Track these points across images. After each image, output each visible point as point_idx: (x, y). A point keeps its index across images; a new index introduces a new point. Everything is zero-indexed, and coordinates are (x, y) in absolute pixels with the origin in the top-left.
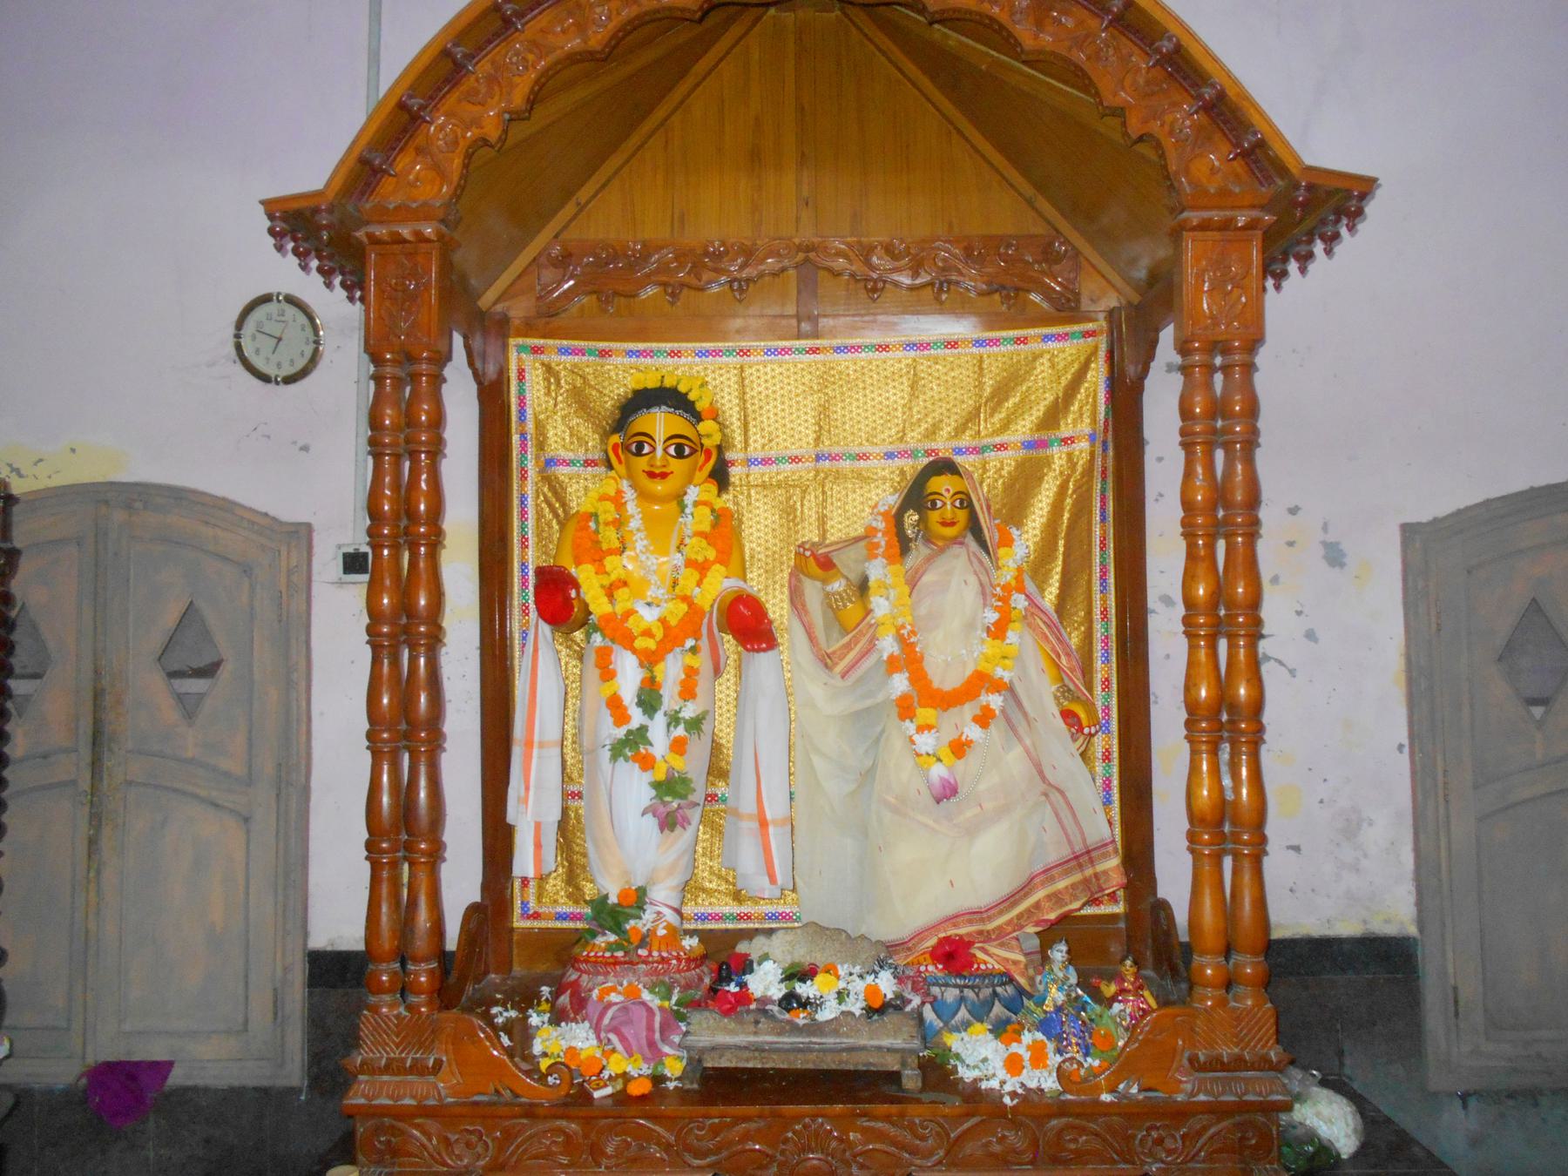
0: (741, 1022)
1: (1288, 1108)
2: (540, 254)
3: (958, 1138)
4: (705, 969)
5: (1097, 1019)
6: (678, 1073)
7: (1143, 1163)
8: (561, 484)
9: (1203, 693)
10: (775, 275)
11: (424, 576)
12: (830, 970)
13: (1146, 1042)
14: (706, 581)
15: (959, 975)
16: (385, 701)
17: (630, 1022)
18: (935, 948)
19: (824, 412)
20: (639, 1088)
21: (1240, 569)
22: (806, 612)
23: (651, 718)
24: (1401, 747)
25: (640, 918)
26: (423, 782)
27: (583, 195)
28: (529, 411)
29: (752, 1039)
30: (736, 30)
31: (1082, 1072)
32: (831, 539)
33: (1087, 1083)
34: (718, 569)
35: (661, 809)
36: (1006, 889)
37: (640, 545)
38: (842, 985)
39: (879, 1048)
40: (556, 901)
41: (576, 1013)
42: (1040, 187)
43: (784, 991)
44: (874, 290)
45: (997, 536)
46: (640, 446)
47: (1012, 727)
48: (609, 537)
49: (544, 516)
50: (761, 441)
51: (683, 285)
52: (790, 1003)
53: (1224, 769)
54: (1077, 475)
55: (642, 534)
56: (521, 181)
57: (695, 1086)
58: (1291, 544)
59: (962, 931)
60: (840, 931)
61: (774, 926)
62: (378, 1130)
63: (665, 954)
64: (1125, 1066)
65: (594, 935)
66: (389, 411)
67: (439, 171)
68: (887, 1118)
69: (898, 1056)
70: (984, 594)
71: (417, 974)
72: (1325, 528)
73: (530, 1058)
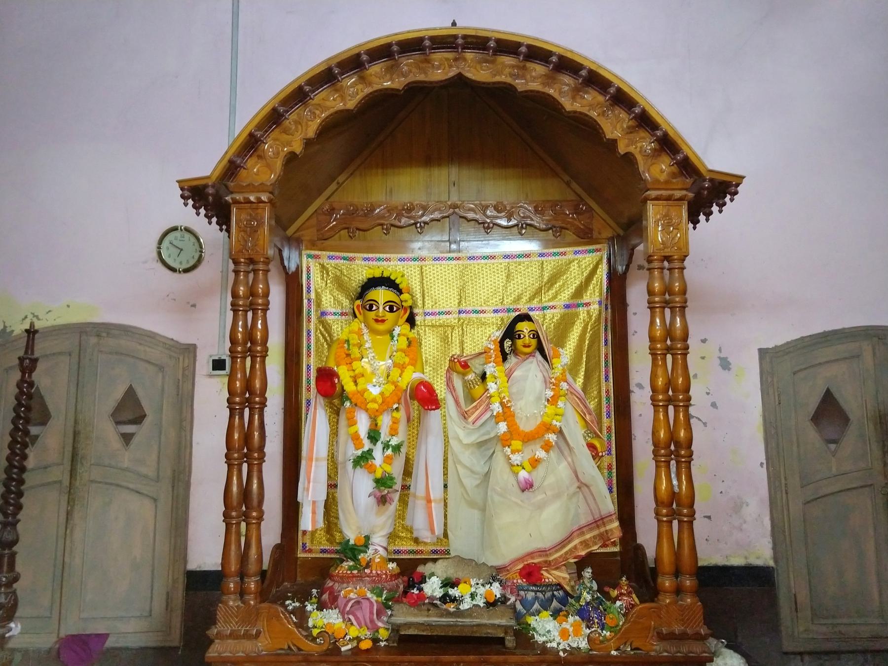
0: (421, 611)
8: (328, 324)
15: (535, 585)
19: (462, 290)
20: (366, 645)
21: (680, 372)
23: (375, 444)
24: (762, 464)
26: (255, 481)
27: (341, 179)
28: (312, 289)
29: (426, 619)
34: (410, 368)
35: (379, 494)
36: (558, 537)
38: (473, 590)
39: (493, 625)
44: (488, 228)
46: (371, 306)
47: (562, 452)
48: (355, 352)
50: (431, 303)
59: (536, 561)
65: (342, 561)
70: (545, 382)
72: (720, 350)
73: (308, 629)
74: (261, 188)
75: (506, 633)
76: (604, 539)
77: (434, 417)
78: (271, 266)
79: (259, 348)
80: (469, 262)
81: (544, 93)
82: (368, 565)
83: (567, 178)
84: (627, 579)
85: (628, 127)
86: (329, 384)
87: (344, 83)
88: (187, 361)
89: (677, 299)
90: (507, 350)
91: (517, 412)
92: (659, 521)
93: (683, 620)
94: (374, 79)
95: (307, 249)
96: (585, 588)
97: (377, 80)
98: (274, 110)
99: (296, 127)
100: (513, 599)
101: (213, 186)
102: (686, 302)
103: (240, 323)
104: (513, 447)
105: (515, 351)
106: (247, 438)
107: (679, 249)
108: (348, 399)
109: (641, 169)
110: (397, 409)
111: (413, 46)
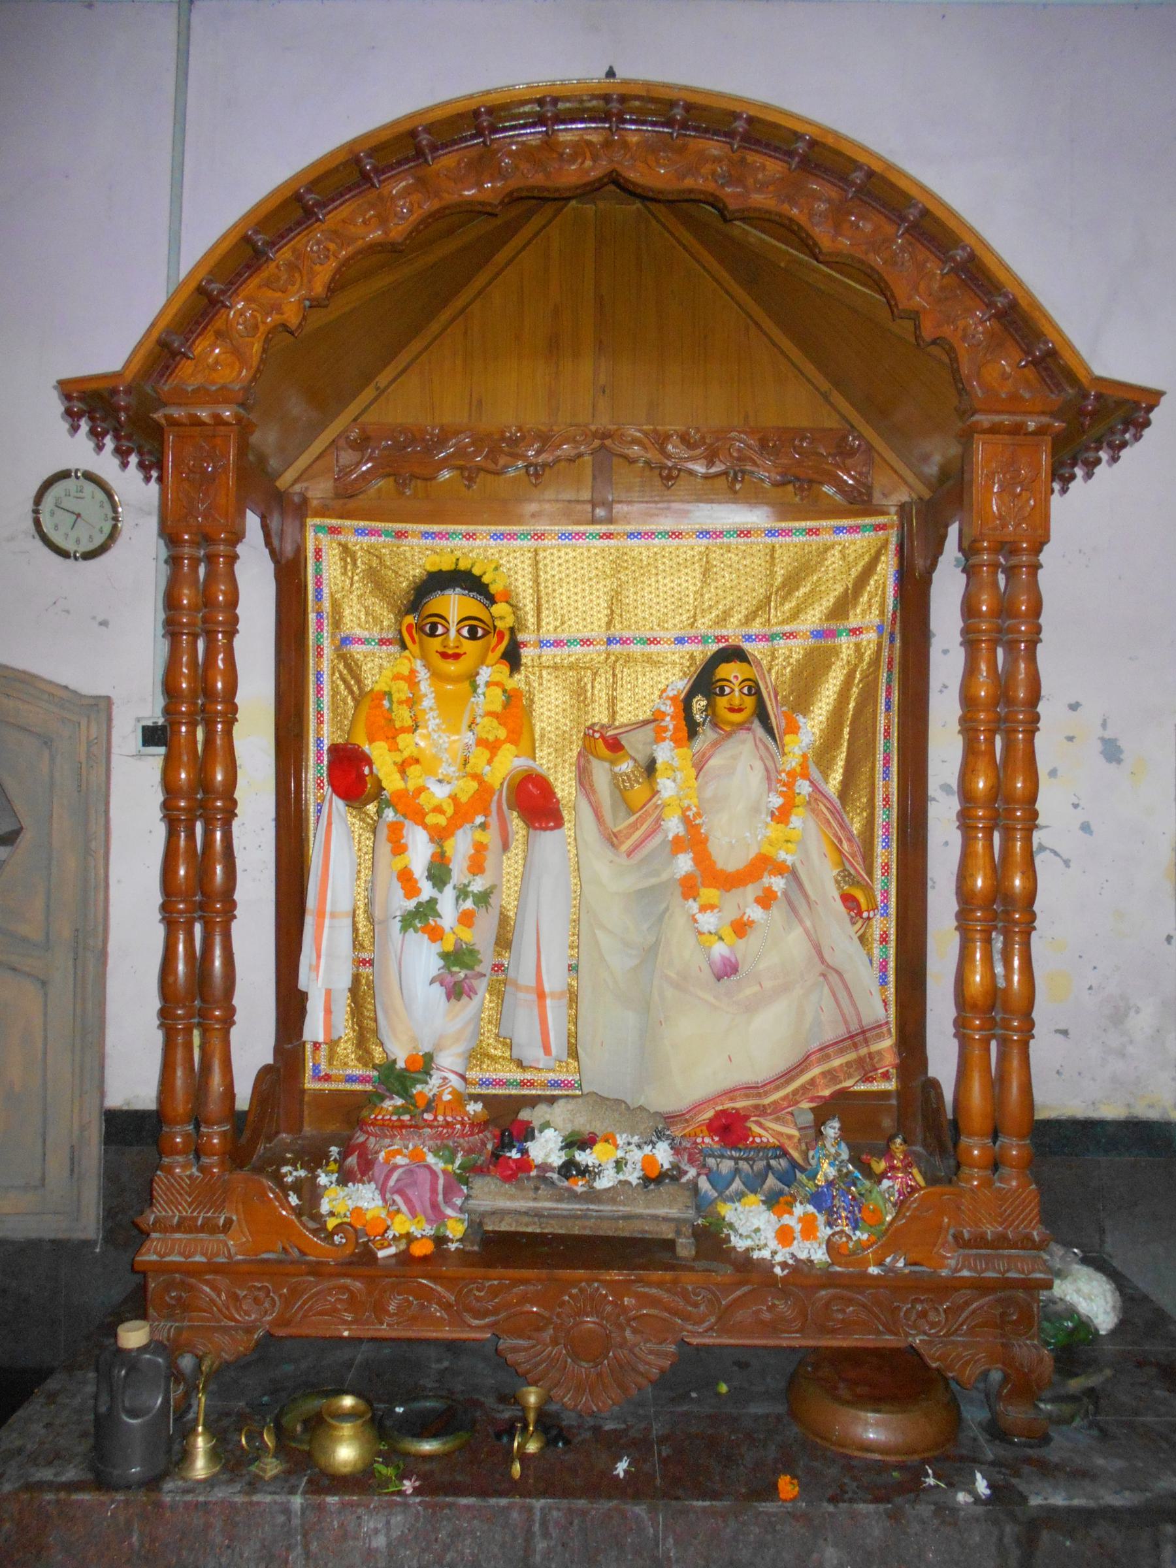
0: (522, 1189)
1: (1049, 1286)
2: (339, 436)
3: (729, 1306)
4: (489, 1135)
5: (867, 1194)
6: (459, 1235)
7: (907, 1335)
8: (356, 661)
9: (979, 883)
10: (571, 460)
12: (609, 1139)
13: (912, 1219)
14: (496, 759)
15: (734, 1147)
16: (182, 872)
17: (414, 1184)
18: (711, 1120)
19: (615, 599)
20: (421, 1249)
21: (1020, 764)
22: (594, 792)
23: (441, 891)
25: (426, 1083)
26: (218, 952)
27: (383, 379)
28: (326, 591)
29: (532, 1204)
30: (536, 222)
31: (851, 1245)
32: (622, 719)
33: (854, 1256)
34: (508, 750)
36: (781, 1064)
37: (432, 724)
38: (620, 1154)
39: (655, 1217)
40: (346, 1064)
41: (363, 1174)
42: (837, 384)
43: (564, 1159)
44: (669, 477)
45: (783, 725)
46: (434, 627)
48: (403, 716)
49: (339, 693)
51: (480, 469)
52: (569, 1171)
53: (997, 957)
54: (865, 665)
55: (435, 714)
56: (319, 366)
57: (476, 1248)
58: (1070, 739)
59: (739, 1105)
60: (618, 1102)
61: (556, 1092)
62: (169, 1286)
63: (449, 1119)
64: (891, 1240)
65: (383, 1099)
66: (186, 591)
67: (237, 353)
68: (660, 1284)
69: (673, 1225)
70: (769, 779)
71: (210, 1137)
72: (1104, 725)
73: (317, 1217)
74: (222, 396)
76: (866, 1068)
90: (698, 718)
93: (1001, 1215)
96: (827, 1156)
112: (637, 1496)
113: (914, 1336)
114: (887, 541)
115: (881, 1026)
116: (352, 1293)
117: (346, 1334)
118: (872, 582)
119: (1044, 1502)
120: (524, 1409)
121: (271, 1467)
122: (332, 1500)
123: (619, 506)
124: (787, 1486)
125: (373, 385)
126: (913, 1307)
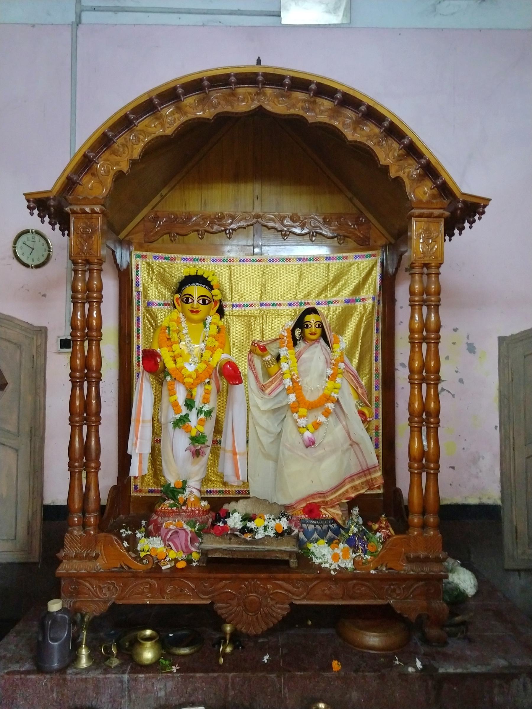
0: (224, 539)
1: (447, 577)
3: (311, 588)
7: (387, 599)
11: (94, 353)
15: (315, 520)
19: (263, 286)
20: (181, 565)
21: (432, 357)
23: (191, 410)
24: (496, 427)
25: (184, 493)
26: (93, 439)
27: (164, 192)
29: (228, 546)
34: (219, 351)
35: (193, 449)
36: (334, 483)
38: (266, 523)
39: (280, 551)
40: (149, 485)
44: (285, 235)
46: (187, 299)
47: (338, 417)
48: (174, 336)
50: (238, 297)
57: (204, 565)
59: (317, 501)
60: (265, 500)
63: (193, 509)
65: (165, 500)
68: (283, 580)
69: (288, 554)
70: (327, 362)
72: (468, 338)
73: (136, 552)
74: (95, 201)
75: (290, 557)
76: (370, 484)
77: (238, 390)
78: (104, 266)
79: (94, 334)
80: (269, 263)
81: (330, 124)
82: (185, 504)
83: (350, 195)
84: (386, 516)
85: (399, 156)
86: (153, 362)
87: (163, 112)
88: (39, 341)
89: (433, 299)
90: (298, 337)
91: (303, 386)
92: (412, 473)
94: (188, 109)
95: (135, 250)
96: (353, 523)
97: (191, 110)
98: (104, 134)
99: (124, 150)
100: (296, 531)
101: (54, 199)
102: (439, 301)
103: (79, 313)
104: (300, 413)
105: (303, 337)
106: (86, 404)
107: (436, 258)
108: (169, 374)
109: (408, 190)
110: (209, 383)
111: (220, 81)
112: (272, 671)
113: (390, 600)
114: (376, 261)
115: (375, 467)
116: (150, 584)
117: (148, 602)
118: (370, 279)
119: (445, 671)
120: (225, 634)
121: (115, 662)
122: (141, 676)
123: (265, 247)
124: (336, 665)
125: (159, 194)
126: (390, 587)
